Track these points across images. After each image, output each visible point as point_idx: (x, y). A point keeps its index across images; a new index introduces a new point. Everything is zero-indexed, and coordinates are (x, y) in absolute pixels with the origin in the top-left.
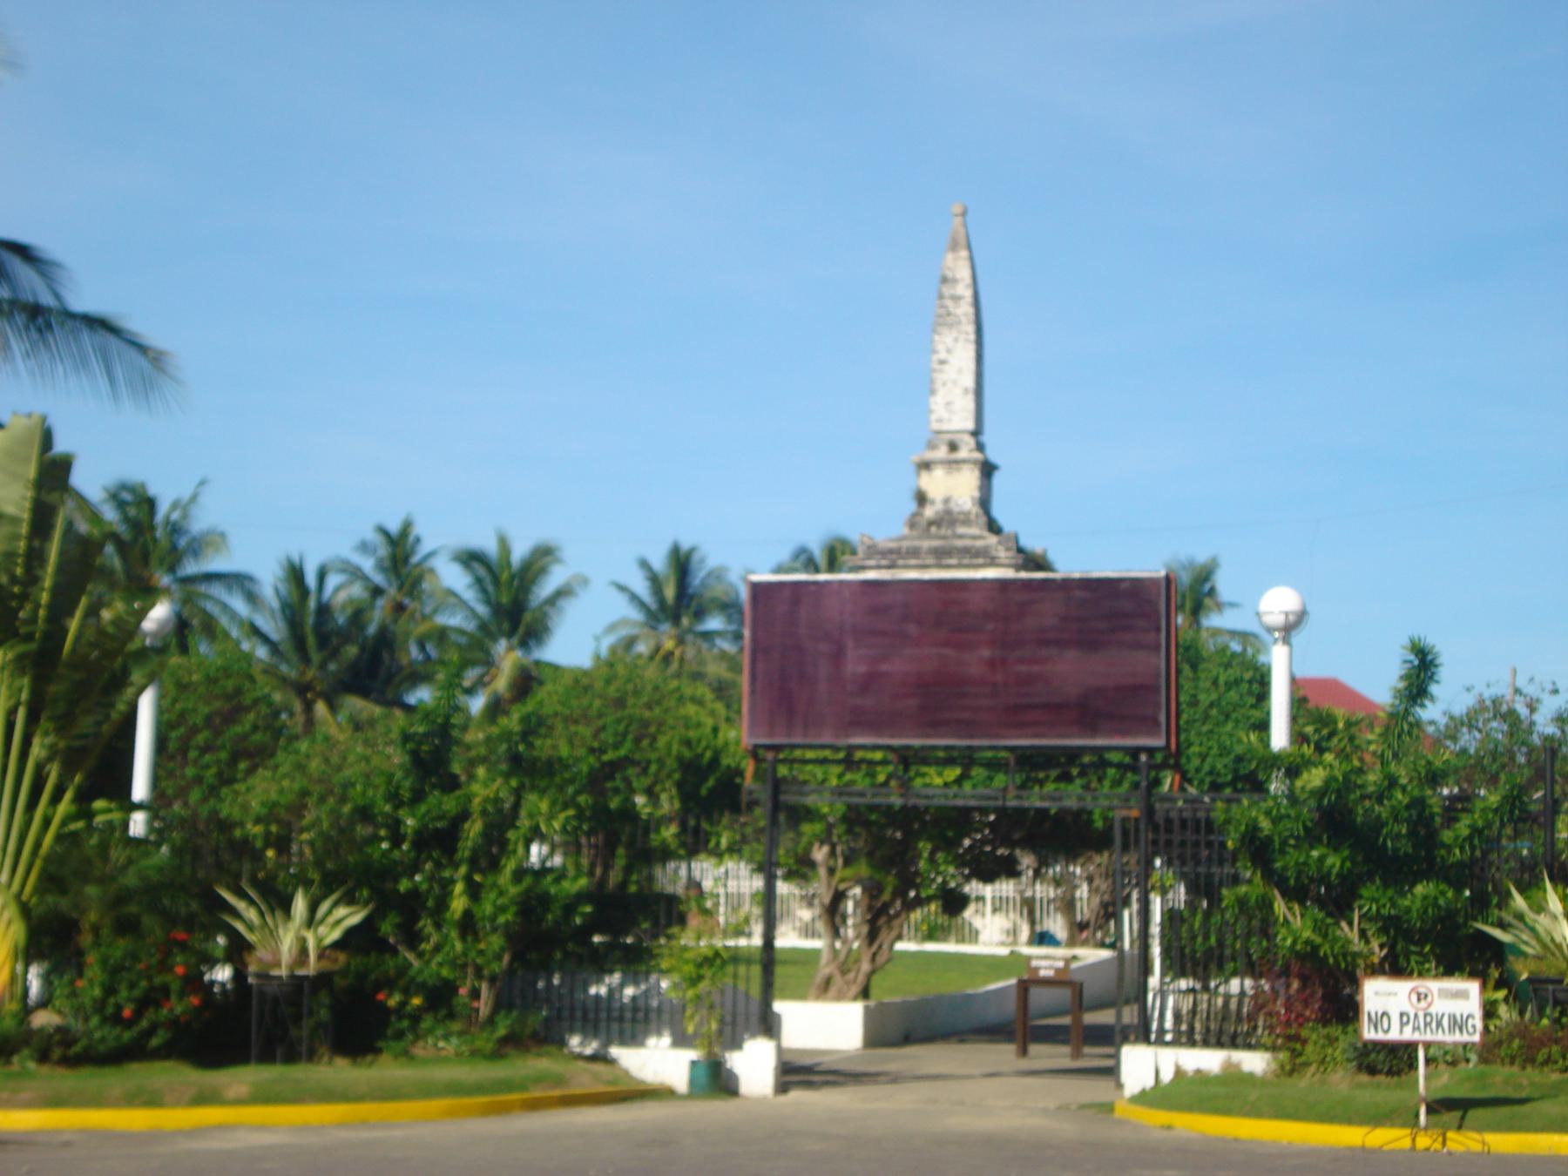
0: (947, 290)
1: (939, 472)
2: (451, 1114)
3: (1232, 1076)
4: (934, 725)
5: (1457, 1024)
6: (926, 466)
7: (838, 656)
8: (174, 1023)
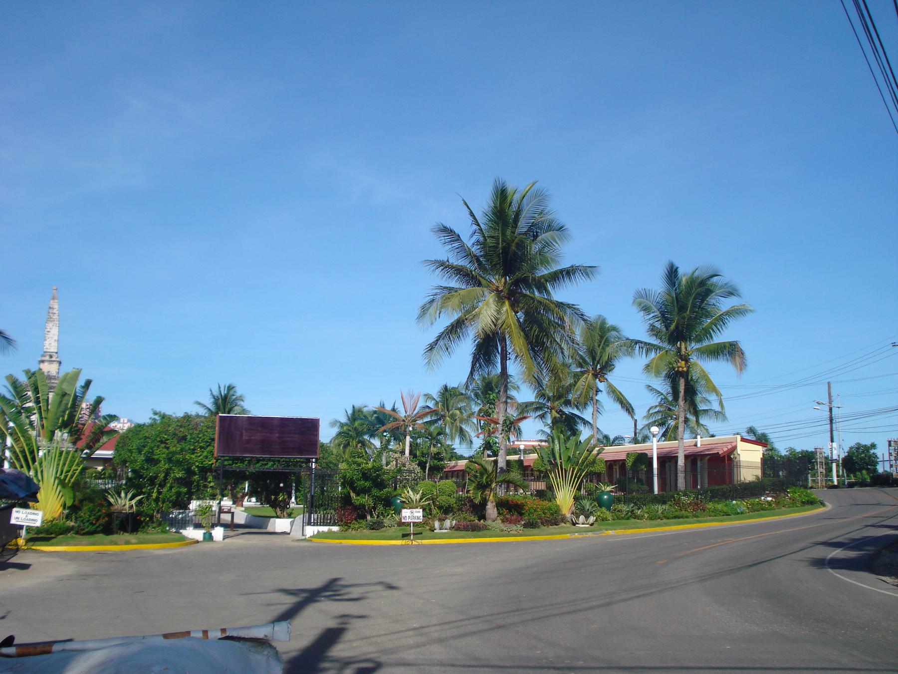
0: (51, 311)
1: (46, 364)
2: (181, 545)
3: (330, 532)
4: (263, 452)
5: (418, 518)
6: (43, 361)
7: (241, 435)
8: (102, 525)
